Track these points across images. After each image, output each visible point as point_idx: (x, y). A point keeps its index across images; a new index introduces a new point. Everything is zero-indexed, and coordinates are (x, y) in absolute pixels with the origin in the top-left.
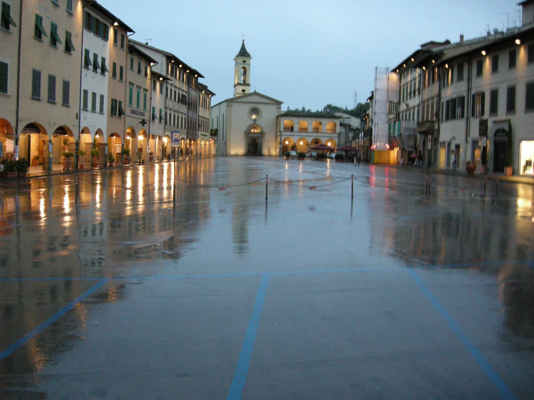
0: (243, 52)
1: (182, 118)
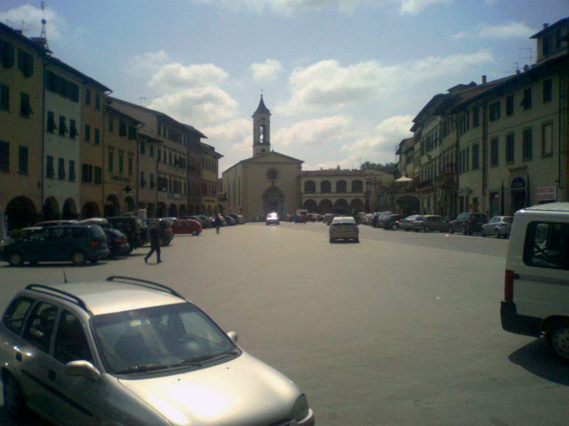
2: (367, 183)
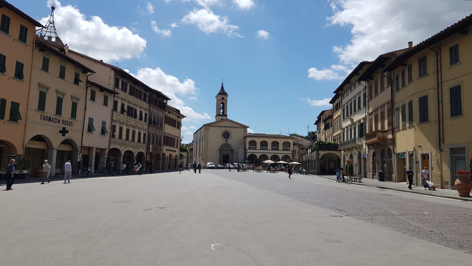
2: (294, 145)
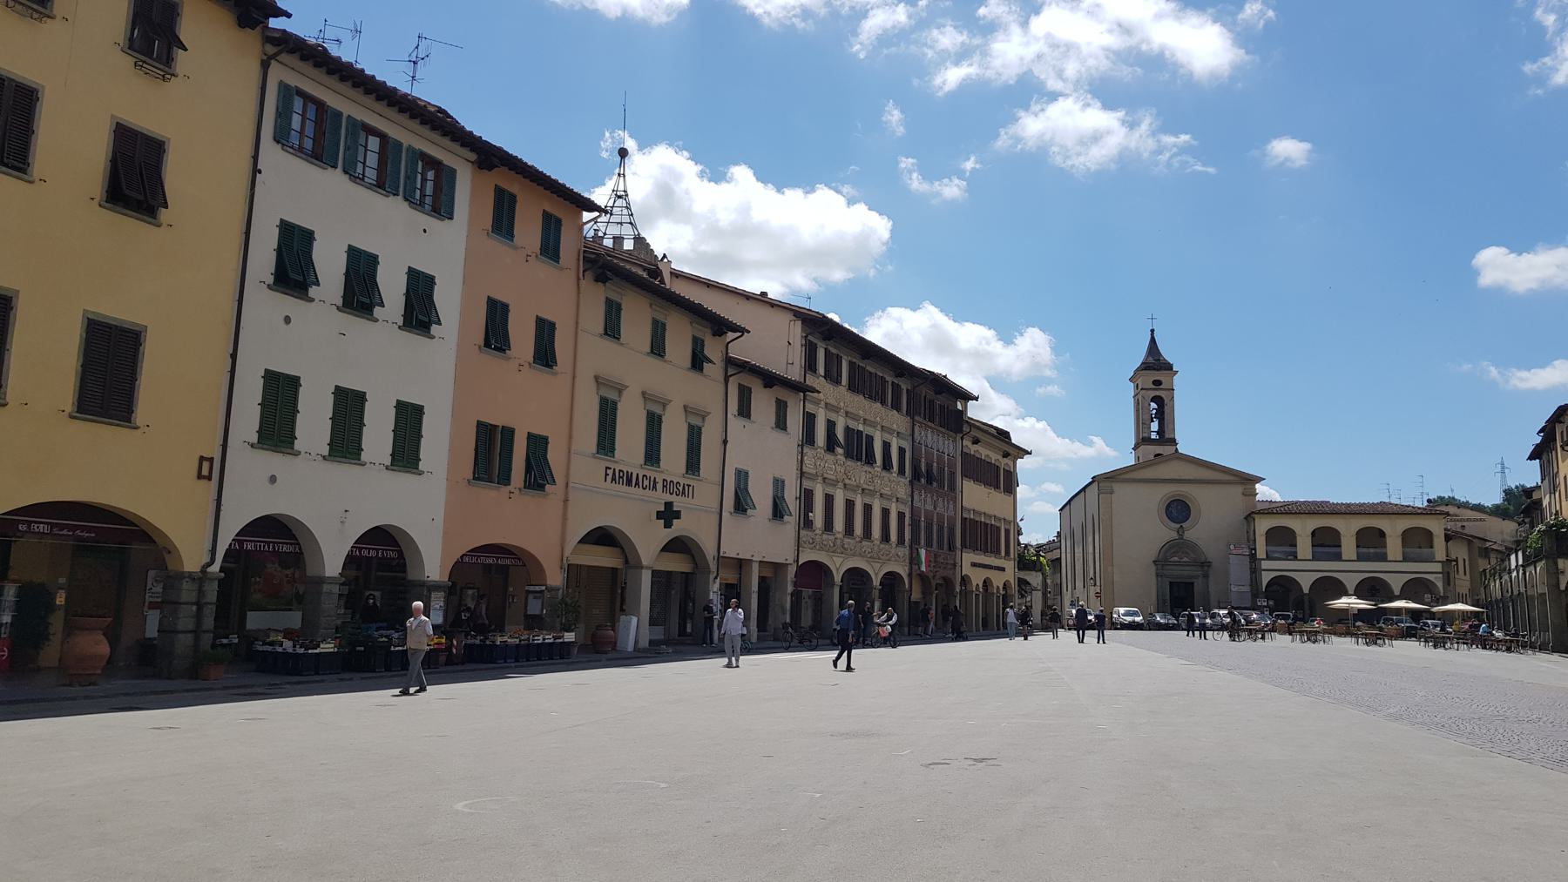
0: (1151, 360)
1: (885, 513)
2: (1448, 538)
